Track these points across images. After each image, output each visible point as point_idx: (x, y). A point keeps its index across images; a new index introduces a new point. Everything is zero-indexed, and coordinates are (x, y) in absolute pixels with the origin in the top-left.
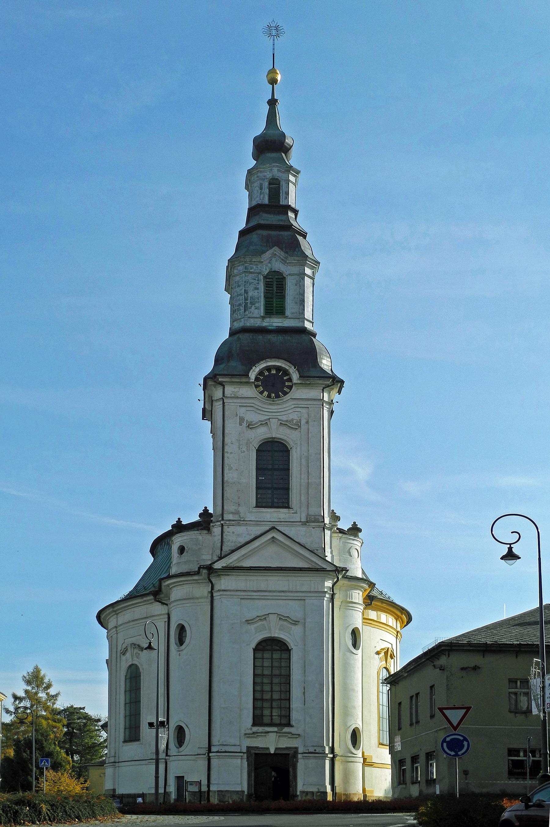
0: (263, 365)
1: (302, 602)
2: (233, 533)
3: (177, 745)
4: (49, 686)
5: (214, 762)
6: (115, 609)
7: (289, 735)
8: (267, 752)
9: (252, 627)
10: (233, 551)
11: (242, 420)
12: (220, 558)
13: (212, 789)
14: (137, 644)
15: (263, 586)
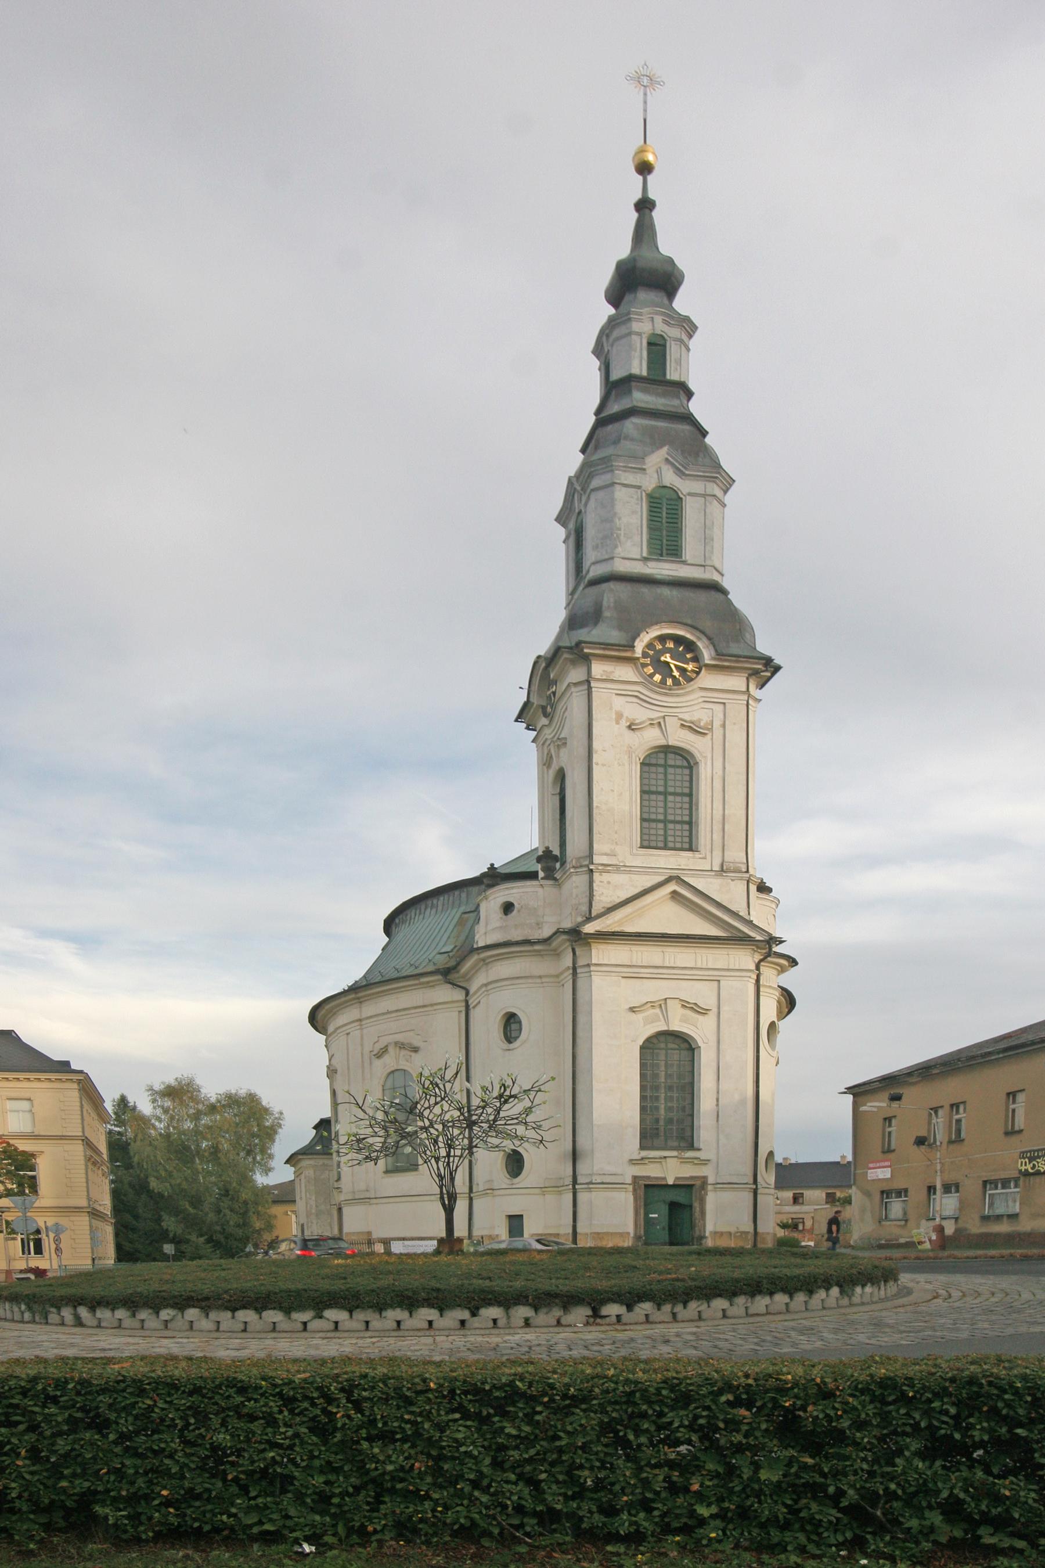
0: (655, 632)
2: (609, 883)
9: (640, 1017)
11: (619, 716)
12: (589, 919)
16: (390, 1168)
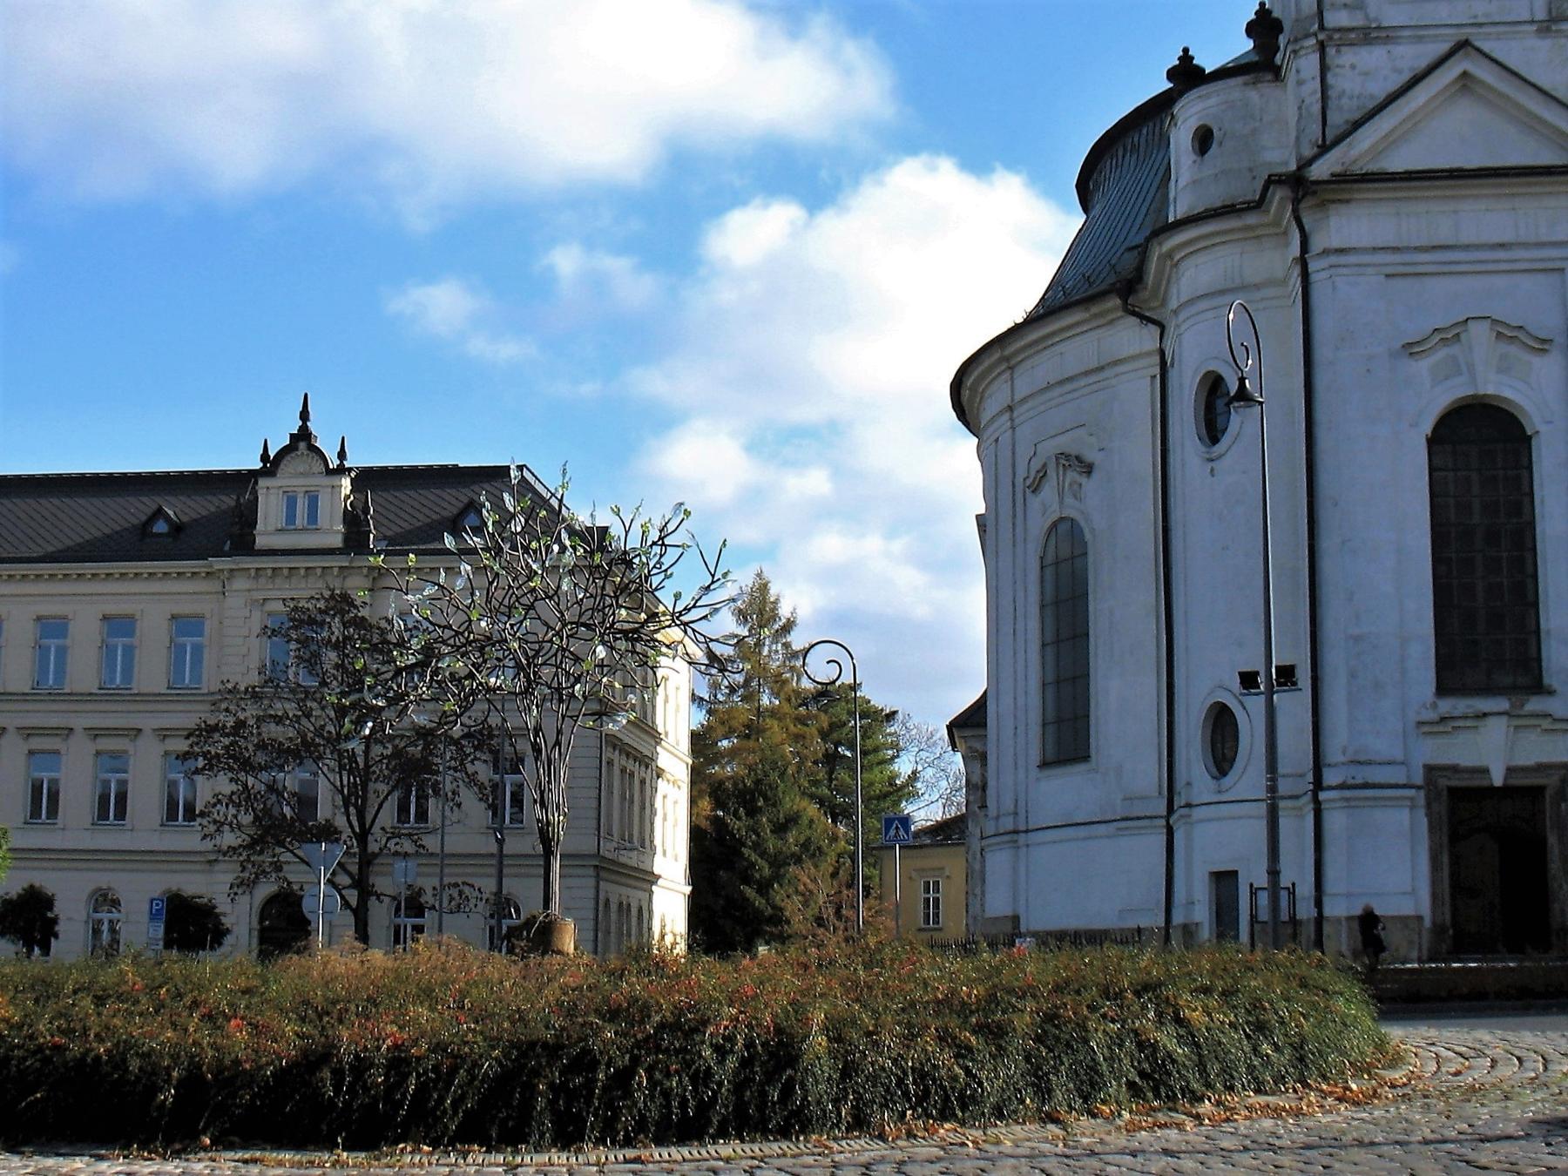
1: (1555, 277)
2: (1353, 67)
3: (1214, 770)
4: (788, 627)
5: (1335, 821)
6: (1007, 352)
7: (1546, 724)
8: (1485, 783)
9: (1422, 366)
10: (1357, 125)
12: (1324, 148)
13: (1328, 911)
14: (1074, 453)
15: (1444, 235)
16: (1050, 757)
